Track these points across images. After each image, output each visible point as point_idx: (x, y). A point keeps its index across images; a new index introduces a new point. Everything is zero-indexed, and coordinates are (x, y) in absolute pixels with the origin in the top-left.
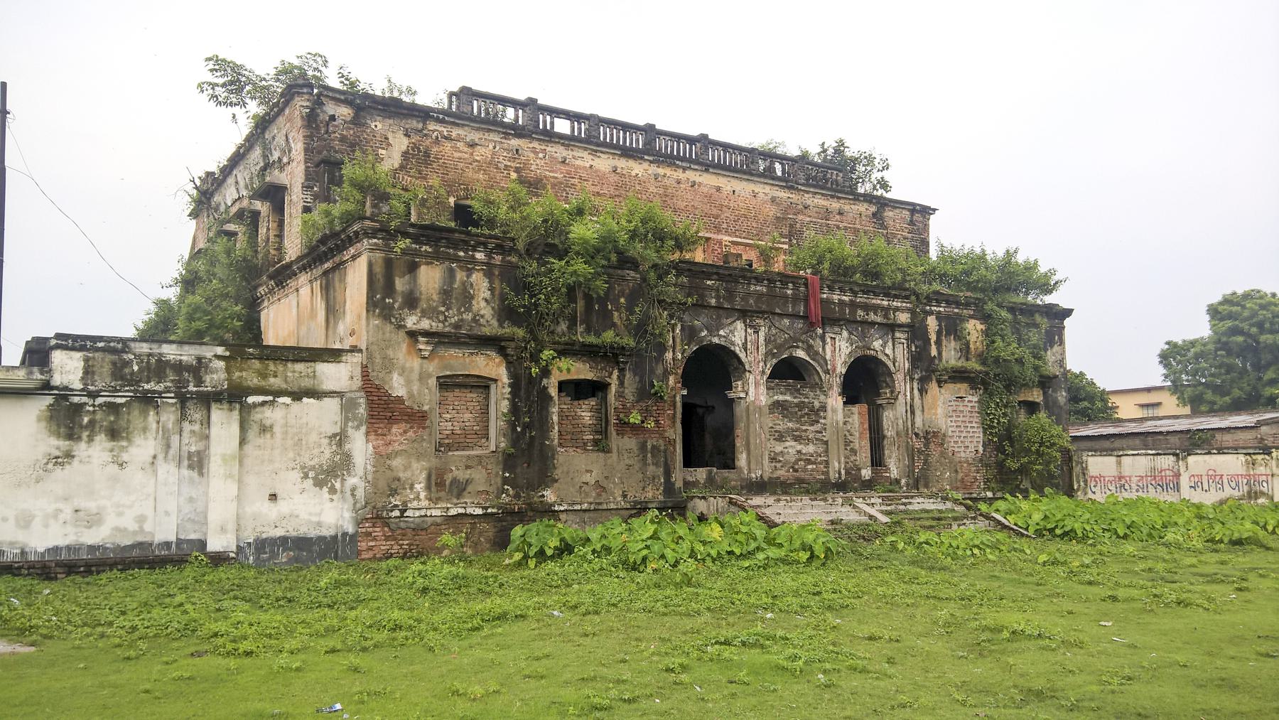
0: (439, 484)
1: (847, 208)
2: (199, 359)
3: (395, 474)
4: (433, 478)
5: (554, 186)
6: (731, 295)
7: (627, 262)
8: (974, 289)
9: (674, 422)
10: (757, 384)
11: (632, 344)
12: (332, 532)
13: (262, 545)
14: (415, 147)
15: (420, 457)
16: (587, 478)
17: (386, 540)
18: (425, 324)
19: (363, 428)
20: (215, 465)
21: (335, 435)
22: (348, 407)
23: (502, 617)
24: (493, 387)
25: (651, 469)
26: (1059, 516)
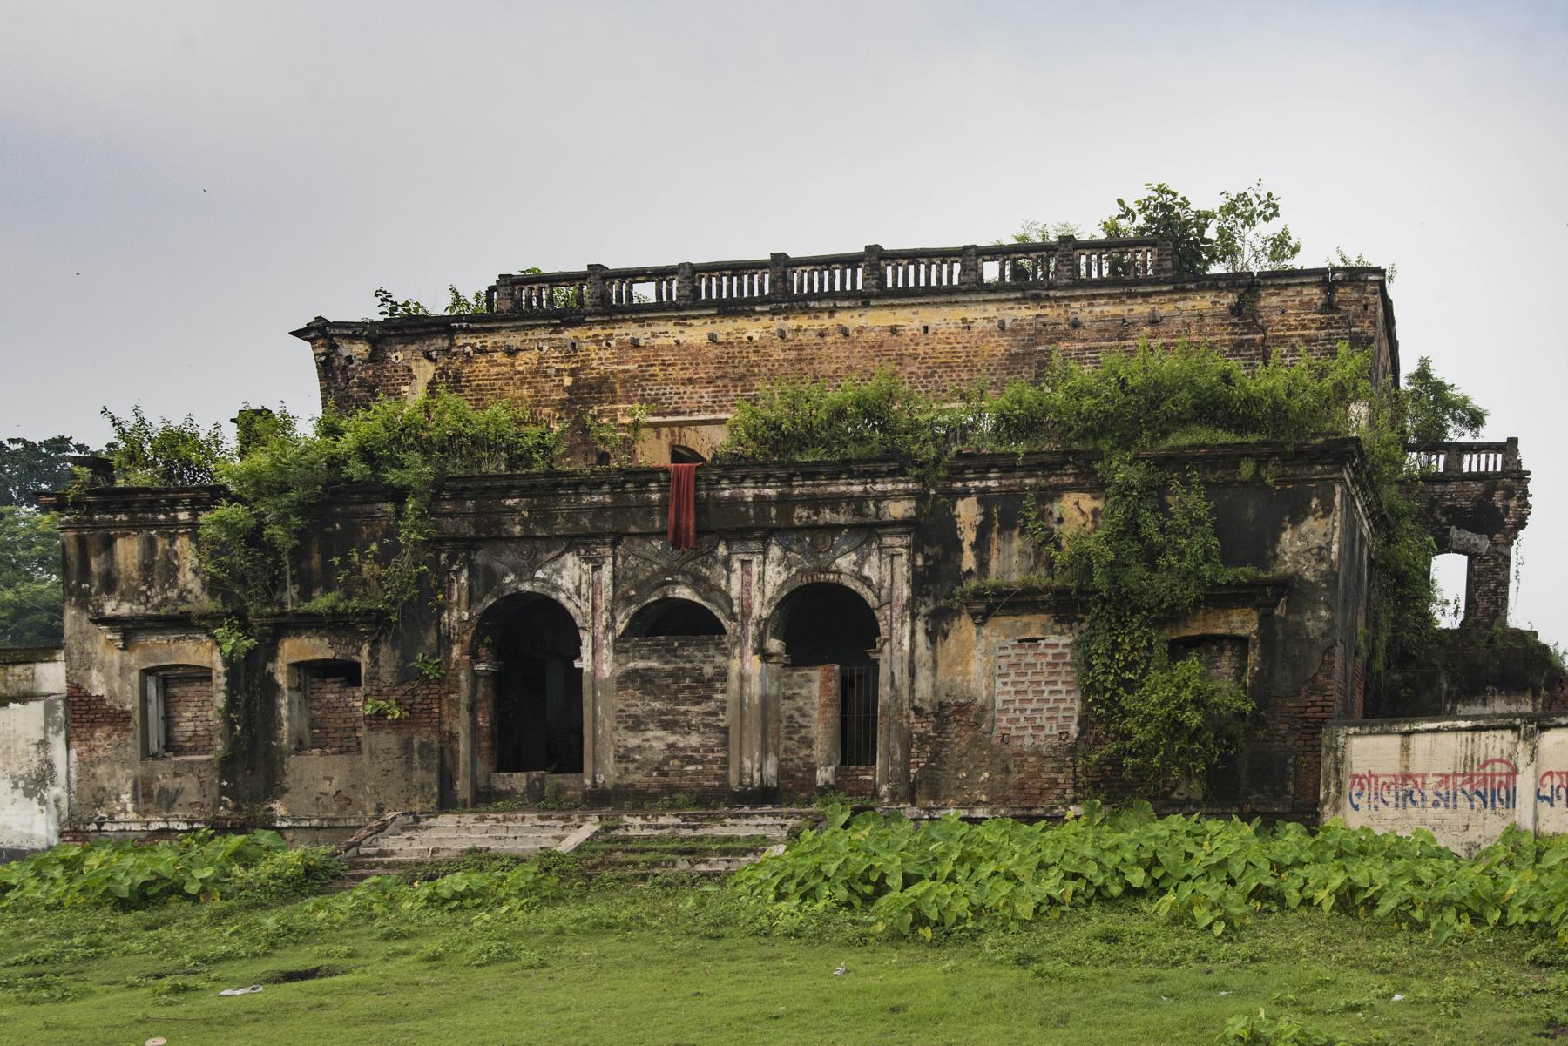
0: (145, 794)
1: (1166, 309)
5: (624, 383)
6: (547, 518)
14: (443, 372)
15: (124, 764)
16: (326, 786)
18: (125, 609)
19: (63, 734)
22: (49, 710)
25: (419, 775)
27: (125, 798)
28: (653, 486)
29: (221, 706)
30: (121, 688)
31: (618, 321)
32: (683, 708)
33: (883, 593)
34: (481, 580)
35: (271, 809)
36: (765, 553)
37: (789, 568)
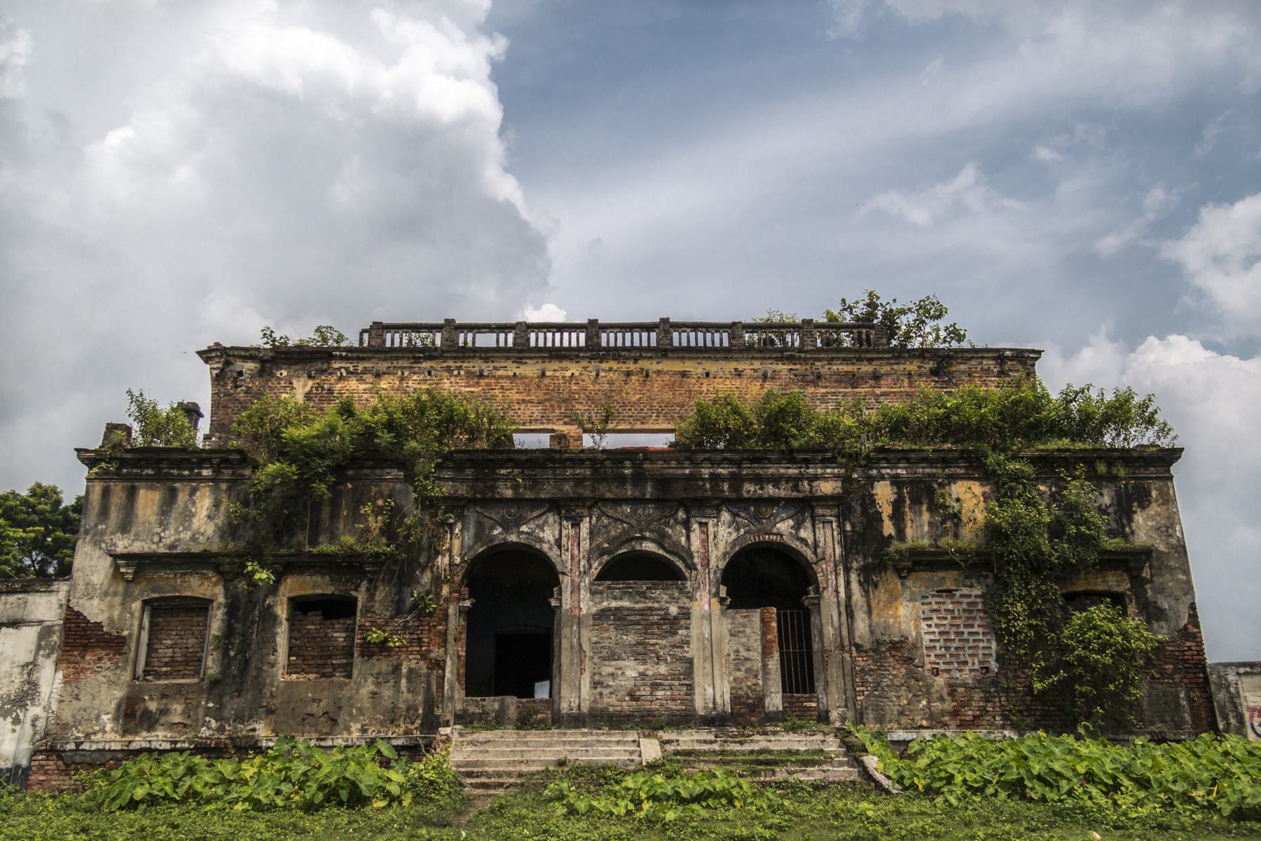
4: (123, 708)
14: (319, 386)
16: (314, 708)
19: (54, 657)
21: (27, 664)
28: (628, 463)
30: (121, 617)
31: (469, 357)
33: (819, 551)
35: (254, 730)
36: (718, 517)
37: (738, 530)
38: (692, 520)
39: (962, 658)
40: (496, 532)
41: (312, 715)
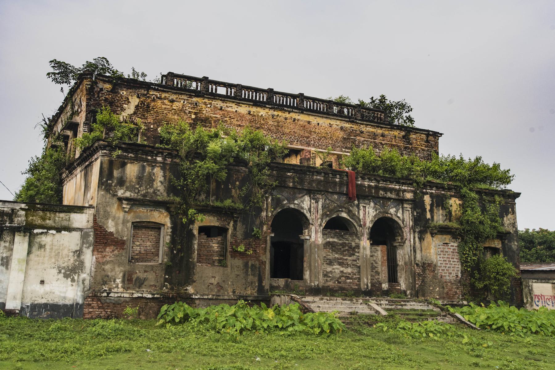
0: (129, 280)
1: (386, 133)
2: (13, 210)
3: (106, 273)
4: (126, 276)
5: (215, 122)
6: (301, 181)
7: (240, 161)
8: (455, 181)
9: (265, 252)
10: (316, 232)
11: (241, 206)
12: (71, 303)
13: (35, 307)
14: (142, 103)
15: (120, 264)
16: (213, 281)
17: (99, 308)
18: (128, 194)
19: (91, 248)
20: (14, 264)
21: (76, 251)
22: (85, 236)
23: (118, 351)
24: (162, 228)
25: (250, 278)
26: (496, 317)
27: (118, 281)
29: (168, 242)
30: (122, 230)
32: (345, 258)
33: (405, 223)
34: (275, 201)
35: (187, 290)
37: (376, 211)
38: (361, 205)
39: (450, 271)
40: (285, 202)
41: (212, 284)
